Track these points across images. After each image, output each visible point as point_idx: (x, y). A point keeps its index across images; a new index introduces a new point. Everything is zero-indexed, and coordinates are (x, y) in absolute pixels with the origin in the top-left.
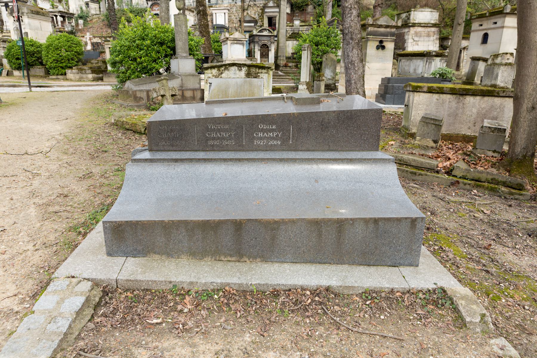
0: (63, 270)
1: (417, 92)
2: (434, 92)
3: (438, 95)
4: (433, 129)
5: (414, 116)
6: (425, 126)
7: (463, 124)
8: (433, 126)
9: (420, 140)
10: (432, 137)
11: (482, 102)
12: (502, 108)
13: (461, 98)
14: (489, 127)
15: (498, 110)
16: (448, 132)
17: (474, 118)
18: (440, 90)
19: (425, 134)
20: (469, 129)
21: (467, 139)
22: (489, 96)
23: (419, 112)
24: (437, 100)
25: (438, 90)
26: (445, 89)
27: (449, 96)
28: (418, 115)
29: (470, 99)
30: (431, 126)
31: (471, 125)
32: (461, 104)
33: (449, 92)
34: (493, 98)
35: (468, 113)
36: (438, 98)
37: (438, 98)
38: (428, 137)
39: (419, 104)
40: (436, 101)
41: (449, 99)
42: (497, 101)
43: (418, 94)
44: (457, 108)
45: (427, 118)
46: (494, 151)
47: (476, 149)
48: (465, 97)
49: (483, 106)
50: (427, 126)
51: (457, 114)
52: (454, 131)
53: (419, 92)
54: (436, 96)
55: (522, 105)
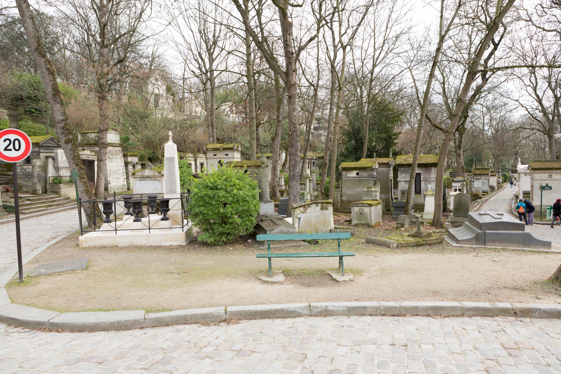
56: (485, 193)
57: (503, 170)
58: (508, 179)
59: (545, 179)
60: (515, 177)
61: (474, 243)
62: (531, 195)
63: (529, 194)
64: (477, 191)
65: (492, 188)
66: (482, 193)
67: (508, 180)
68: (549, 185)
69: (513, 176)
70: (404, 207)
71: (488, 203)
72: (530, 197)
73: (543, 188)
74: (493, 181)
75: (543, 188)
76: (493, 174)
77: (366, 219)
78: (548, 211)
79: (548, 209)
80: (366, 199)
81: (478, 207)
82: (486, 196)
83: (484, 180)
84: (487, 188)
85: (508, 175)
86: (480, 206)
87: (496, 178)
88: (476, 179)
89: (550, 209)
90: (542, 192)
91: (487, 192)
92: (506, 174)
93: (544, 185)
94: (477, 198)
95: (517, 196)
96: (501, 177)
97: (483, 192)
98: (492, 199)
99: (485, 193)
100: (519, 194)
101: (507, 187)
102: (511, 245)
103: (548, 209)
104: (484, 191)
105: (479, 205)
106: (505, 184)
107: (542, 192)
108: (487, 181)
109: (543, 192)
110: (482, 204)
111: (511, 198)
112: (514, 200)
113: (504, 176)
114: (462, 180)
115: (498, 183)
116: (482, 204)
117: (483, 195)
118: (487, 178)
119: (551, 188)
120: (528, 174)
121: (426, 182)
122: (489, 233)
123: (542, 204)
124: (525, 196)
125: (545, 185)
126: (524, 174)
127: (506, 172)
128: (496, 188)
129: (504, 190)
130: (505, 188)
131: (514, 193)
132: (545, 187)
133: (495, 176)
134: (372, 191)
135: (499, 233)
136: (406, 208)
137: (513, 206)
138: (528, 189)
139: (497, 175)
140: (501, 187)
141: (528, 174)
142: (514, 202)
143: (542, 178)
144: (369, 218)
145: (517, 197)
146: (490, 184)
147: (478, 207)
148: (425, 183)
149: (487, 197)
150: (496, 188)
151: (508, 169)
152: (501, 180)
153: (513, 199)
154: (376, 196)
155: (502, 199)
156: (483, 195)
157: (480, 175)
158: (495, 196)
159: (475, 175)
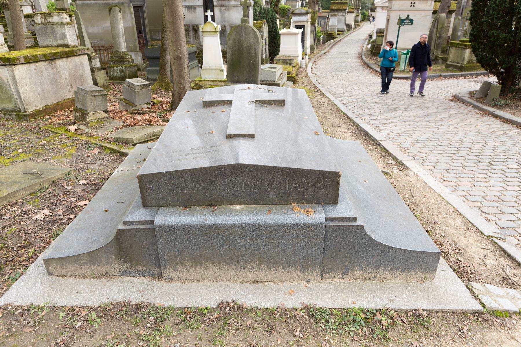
0: (470, 305)
1: (15, 65)
2: (31, 61)
3: (34, 64)
4: (101, 100)
5: (23, 94)
6: (94, 100)
7: (64, 89)
8: (101, 97)
9: (93, 115)
10: (102, 108)
11: (68, 63)
12: (82, 65)
13: (53, 63)
14: (140, 85)
15: (81, 68)
16: (57, 101)
17: (69, 81)
18: (35, 59)
19: (95, 108)
20: (70, 92)
21: (72, 101)
22: (70, 56)
23: (26, 88)
24: (36, 69)
25: (34, 58)
26: (39, 56)
27: (43, 63)
28: (26, 92)
29: (60, 63)
30: (99, 98)
31: (69, 87)
32: (55, 69)
33: (43, 59)
34: (74, 57)
35: (64, 77)
36: (36, 68)
37: (36, 68)
38: (99, 109)
39: (22, 79)
40: (35, 71)
41: (44, 66)
42: (77, 59)
43: (16, 67)
44: (54, 74)
45: (93, 91)
46: (147, 104)
47: (136, 106)
48: (54, 61)
49: (70, 67)
50: (96, 99)
51: (56, 81)
52: (60, 98)
53: (17, 64)
54: (33, 66)
55: (184, 63)
56: (341, 32)
57: (363, 8)
58: (367, 18)
59: (405, 8)
60: (373, 16)
61: (115, 267)
62: (384, 34)
63: (383, 33)
64: (332, 30)
65: (348, 27)
66: (337, 33)
67: (365, 18)
68: (411, 17)
69: (371, 15)
70: (158, 58)
71: (340, 44)
72: (383, 36)
73: (401, 22)
74: (351, 19)
75: (401, 22)
76: (352, 10)
77: (10, 98)
78: (403, 56)
79: (404, 54)
80: (45, 44)
81: (327, 49)
82: (341, 36)
83: (341, 17)
84: (343, 27)
85: (367, 13)
86: (331, 48)
87: (354, 15)
88: (332, 15)
89: (407, 54)
90: (399, 27)
91: (342, 31)
92: (365, 12)
93: (404, 17)
94: (331, 38)
95: (372, 35)
96: (360, 15)
97: (338, 31)
98: (346, 39)
99: (341, 32)
100: (373, 33)
101: (364, 26)
102: (272, 273)
103: (404, 54)
104: (340, 30)
105: (330, 47)
106: (363, 23)
107: (399, 27)
108: (344, 18)
109: (402, 27)
110: (333, 46)
111: (365, 38)
112: (367, 41)
113: (363, 14)
114: (305, 12)
115: (356, 21)
116: (331, 47)
117: (338, 34)
118: (344, 14)
119: (412, 21)
120: (385, 8)
121: (223, 9)
122: (172, 229)
123: (398, 46)
124: (379, 34)
125: (405, 17)
126: (380, 8)
127: (366, 10)
128: (353, 26)
129: (360, 30)
130: (362, 26)
131: (369, 32)
132: (405, 20)
133: (353, 12)
134: (53, 24)
135: (216, 228)
136: (161, 60)
137: (364, 48)
138: (383, 26)
139: (355, 12)
140: (359, 25)
141: (385, 8)
142: (366, 43)
143: (402, 8)
144: (15, 96)
145: (371, 36)
146: (347, 22)
147: (327, 49)
148: (220, 10)
149: (342, 37)
150: (353, 26)
151: (368, 6)
152: (359, 19)
153: (366, 39)
154: (64, 36)
155: (355, 40)
156: (338, 34)
157: (337, 10)
158: (350, 36)
159: (333, 10)
